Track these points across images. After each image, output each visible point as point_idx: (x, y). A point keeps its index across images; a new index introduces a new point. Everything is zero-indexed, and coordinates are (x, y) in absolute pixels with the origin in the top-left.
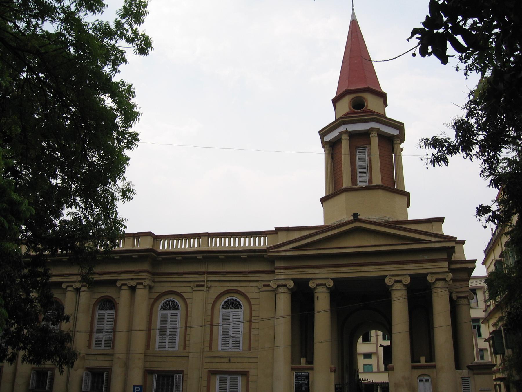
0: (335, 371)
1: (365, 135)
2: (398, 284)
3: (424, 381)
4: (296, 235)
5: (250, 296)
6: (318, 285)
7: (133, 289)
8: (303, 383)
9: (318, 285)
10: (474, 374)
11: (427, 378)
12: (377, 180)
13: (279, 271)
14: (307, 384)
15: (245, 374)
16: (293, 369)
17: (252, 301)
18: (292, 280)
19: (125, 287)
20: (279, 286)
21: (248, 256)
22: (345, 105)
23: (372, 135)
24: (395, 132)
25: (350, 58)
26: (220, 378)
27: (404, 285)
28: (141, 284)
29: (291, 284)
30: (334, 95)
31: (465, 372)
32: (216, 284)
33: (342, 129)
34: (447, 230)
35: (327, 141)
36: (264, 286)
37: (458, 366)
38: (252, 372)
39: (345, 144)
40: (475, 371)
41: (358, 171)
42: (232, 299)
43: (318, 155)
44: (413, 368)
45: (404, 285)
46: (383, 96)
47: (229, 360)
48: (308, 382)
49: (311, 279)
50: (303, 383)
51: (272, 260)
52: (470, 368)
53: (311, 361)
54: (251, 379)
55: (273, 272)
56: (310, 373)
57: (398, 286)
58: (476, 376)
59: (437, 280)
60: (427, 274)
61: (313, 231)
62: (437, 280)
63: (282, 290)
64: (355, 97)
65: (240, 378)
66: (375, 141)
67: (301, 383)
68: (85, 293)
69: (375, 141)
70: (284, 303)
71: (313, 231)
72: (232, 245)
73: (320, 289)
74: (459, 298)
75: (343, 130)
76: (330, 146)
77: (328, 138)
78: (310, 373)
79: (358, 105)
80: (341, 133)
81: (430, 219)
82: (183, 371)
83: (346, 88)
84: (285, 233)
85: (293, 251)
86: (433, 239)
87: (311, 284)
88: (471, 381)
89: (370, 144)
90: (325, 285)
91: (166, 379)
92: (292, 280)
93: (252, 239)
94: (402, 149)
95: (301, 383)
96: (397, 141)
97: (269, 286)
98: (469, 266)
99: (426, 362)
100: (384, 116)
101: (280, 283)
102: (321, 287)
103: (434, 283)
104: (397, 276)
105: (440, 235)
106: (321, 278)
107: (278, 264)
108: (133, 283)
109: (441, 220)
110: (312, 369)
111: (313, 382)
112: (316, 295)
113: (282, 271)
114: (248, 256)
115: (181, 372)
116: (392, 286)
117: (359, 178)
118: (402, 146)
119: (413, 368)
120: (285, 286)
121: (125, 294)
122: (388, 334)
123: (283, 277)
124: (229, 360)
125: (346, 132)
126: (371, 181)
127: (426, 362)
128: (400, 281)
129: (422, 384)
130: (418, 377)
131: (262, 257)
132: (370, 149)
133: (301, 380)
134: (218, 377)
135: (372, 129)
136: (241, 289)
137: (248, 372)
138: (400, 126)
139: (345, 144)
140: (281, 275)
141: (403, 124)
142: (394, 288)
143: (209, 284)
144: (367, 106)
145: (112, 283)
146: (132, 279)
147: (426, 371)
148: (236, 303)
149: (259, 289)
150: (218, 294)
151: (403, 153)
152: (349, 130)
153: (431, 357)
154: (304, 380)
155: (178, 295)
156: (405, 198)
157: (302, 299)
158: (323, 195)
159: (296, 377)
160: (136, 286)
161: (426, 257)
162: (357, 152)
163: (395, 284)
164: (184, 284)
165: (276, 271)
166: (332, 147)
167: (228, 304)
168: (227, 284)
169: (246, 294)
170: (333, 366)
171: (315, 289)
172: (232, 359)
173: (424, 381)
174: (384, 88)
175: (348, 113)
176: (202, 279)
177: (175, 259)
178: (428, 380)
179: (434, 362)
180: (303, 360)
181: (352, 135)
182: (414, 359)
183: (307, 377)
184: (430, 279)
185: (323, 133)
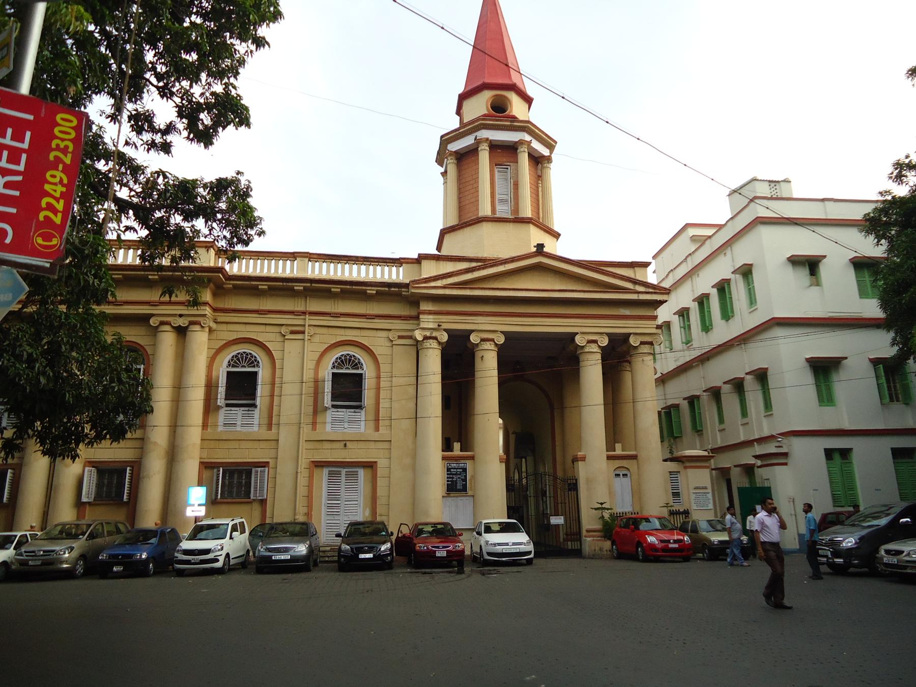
1: (511, 149)
6: (590, 342)
7: (182, 332)
10: (686, 468)
11: (625, 472)
14: (465, 480)
15: (370, 466)
16: (444, 458)
18: (445, 330)
19: (167, 328)
20: (483, 340)
21: (377, 291)
22: (479, 106)
24: (545, 152)
26: (330, 473)
27: (599, 346)
28: (198, 323)
29: (444, 337)
30: (461, 89)
32: (324, 330)
35: (454, 150)
36: (400, 337)
38: (382, 463)
39: (484, 156)
40: (688, 464)
45: (599, 346)
49: (473, 331)
51: (414, 301)
55: (417, 318)
57: (594, 348)
58: (690, 471)
59: (642, 343)
60: (628, 335)
61: (474, 264)
62: (642, 343)
64: (496, 95)
65: (361, 472)
66: (524, 159)
67: (455, 478)
69: (524, 159)
70: (433, 361)
71: (474, 264)
76: (457, 159)
77: (454, 147)
78: (469, 465)
80: (478, 142)
82: (268, 463)
84: (433, 263)
88: (681, 478)
90: (493, 340)
91: (236, 476)
101: (428, 334)
104: (591, 333)
106: (489, 331)
107: (424, 306)
108: (182, 322)
110: (472, 458)
111: (473, 477)
113: (431, 317)
114: (377, 291)
115: (265, 465)
117: (499, 207)
119: (609, 458)
121: (168, 339)
123: (431, 326)
124: (345, 445)
126: (516, 210)
128: (595, 342)
131: (399, 295)
134: (326, 471)
135: (521, 142)
136: (365, 342)
137: (376, 462)
140: (428, 321)
142: (587, 350)
143: (313, 330)
144: (511, 111)
145: (144, 319)
146: (181, 316)
148: (346, 360)
150: (326, 346)
157: (458, 359)
159: (448, 470)
160: (187, 328)
162: (496, 170)
164: (269, 328)
167: (342, 361)
168: (342, 331)
172: (348, 443)
175: (485, 115)
176: (301, 322)
177: (256, 288)
181: (495, 147)
183: (465, 470)
184: (634, 341)
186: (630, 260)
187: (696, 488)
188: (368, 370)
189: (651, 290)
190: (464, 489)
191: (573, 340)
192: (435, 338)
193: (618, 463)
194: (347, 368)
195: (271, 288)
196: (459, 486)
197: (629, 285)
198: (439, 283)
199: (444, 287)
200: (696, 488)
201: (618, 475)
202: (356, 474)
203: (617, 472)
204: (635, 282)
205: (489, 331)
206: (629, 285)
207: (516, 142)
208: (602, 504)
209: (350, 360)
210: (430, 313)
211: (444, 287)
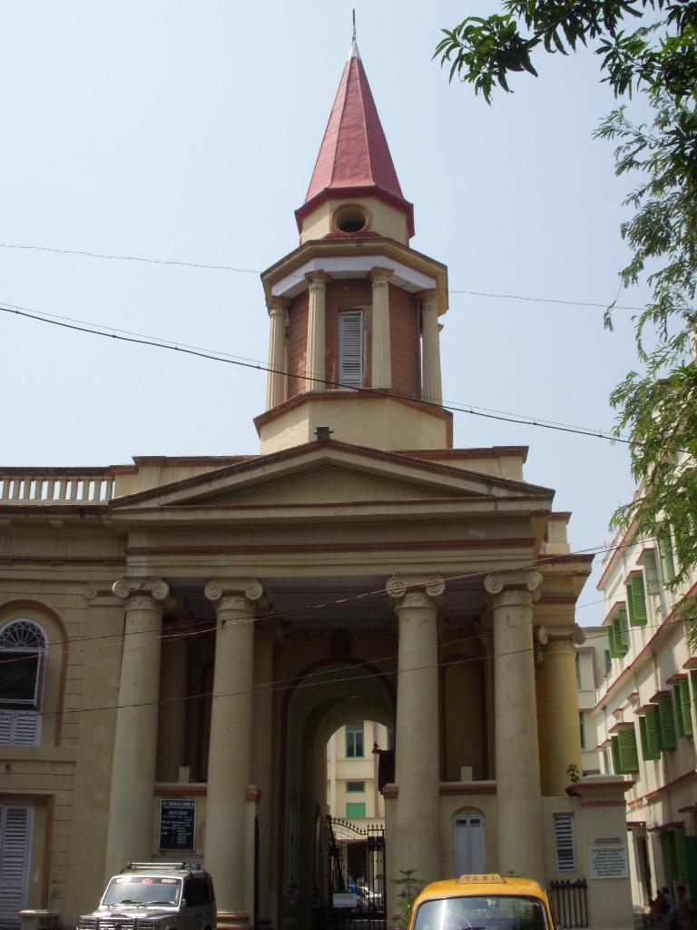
0: (258, 799)
1: (362, 285)
2: (416, 596)
3: (468, 822)
4: (183, 475)
5: (66, 617)
6: (227, 594)
8: (181, 825)
9: (227, 594)
11: (475, 817)
12: (381, 377)
13: (136, 558)
14: (190, 829)
15: (44, 801)
16: (157, 792)
17: (70, 631)
18: (165, 579)
22: (321, 227)
23: (376, 282)
24: (421, 282)
25: (341, 129)
29: (162, 591)
30: (300, 204)
31: (561, 803)
33: (311, 267)
34: (532, 474)
35: (278, 294)
36: (101, 594)
37: (547, 788)
38: (61, 797)
39: (314, 302)
41: (342, 360)
42: (23, 623)
43: (260, 329)
44: (444, 792)
46: (407, 209)
47: (8, 767)
48: (192, 824)
49: (210, 579)
50: (181, 825)
51: (121, 535)
52: (571, 792)
53: (200, 774)
54: (58, 813)
56: (198, 800)
60: (483, 576)
62: (507, 588)
63: (139, 603)
65: (32, 813)
66: (380, 298)
67: (175, 825)
68: (140, 614)
69: (380, 298)
72: (32, 496)
73: (231, 604)
74: (552, 639)
75: (313, 270)
76: (284, 307)
77: (280, 289)
79: (350, 224)
81: (495, 448)
83: (327, 186)
85: (174, 510)
86: (502, 493)
87: (211, 593)
89: (370, 302)
90: (242, 594)
92: (165, 579)
93: (92, 484)
94: (441, 327)
95: (175, 825)
96: (432, 304)
97: (109, 593)
98: (580, 567)
99: (474, 779)
100: (406, 247)
101: (136, 586)
102: (233, 600)
103: (499, 596)
105: (516, 483)
109: (520, 453)
111: (203, 824)
112: (221, 616)
113: (144, 558)
116: (401, 599)
118: (441, 320)
119: (444, 792)
120: (148, 594)
122: (483, 576)
123: (144, 573)
124: (8, 767)
125: (321, 273)
126: (368, 381)
127: (475, 778)
129: (461, 831)
130: (456, 813)
132: (371, 314)
133: (177, 819)
135: (377, 271)
136: (47, 602)
137: (50, 797)
138: (436, 271)
139: (314, 302)
140: (139, 567)
141: (444, 268)
147: (475, 801)
148: (20, 632)
149: (89, 600)
151: (442, 334)
152: (327, 269)
153: (485, 767)
154: (183, 820)
155: (36, 609)
156: (443, 424)
158: (262, 409)
159: (165, 811)
161: (481, 535)
163: (409, 595)
165: (129, 559)
166: (288, 309)
168: (14, 588)
169: (55, 610)
170: (252, 787)
171: (218, 602)
172: (14, 767)
173: (468, 822)
174: (408, 195)
178: (478, 821)
179: (494, 778)
180: (184, 772)
182: (447, 770)
183: (191, 813)
184: (491, 587)
185: (271, 278)
186: (106, 464)
187: (599, 841)
188: (50, 652)
189: (519, 495)
190: (189, 844)
191: (201, 590)
192: (148, 594)
193: (463, 801)
194: (21, 645)
195: (67, 524)
196: (181, 839)
197: (481, 488)
198: (154, 503)
199: (161, 509)
200: (599, 841)
201: (463, 822)
202: (22, 814)
203: (462, 817)
204: (490, 481)
205: (236, 581)
206: (481, 488)
207: (370, 272)
208: (409, 872)
209: (14, 634)
210: (142, 552)
211: (161, 509)
